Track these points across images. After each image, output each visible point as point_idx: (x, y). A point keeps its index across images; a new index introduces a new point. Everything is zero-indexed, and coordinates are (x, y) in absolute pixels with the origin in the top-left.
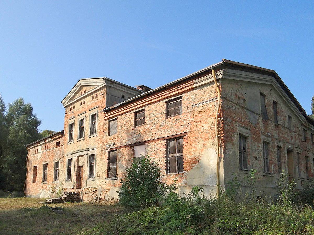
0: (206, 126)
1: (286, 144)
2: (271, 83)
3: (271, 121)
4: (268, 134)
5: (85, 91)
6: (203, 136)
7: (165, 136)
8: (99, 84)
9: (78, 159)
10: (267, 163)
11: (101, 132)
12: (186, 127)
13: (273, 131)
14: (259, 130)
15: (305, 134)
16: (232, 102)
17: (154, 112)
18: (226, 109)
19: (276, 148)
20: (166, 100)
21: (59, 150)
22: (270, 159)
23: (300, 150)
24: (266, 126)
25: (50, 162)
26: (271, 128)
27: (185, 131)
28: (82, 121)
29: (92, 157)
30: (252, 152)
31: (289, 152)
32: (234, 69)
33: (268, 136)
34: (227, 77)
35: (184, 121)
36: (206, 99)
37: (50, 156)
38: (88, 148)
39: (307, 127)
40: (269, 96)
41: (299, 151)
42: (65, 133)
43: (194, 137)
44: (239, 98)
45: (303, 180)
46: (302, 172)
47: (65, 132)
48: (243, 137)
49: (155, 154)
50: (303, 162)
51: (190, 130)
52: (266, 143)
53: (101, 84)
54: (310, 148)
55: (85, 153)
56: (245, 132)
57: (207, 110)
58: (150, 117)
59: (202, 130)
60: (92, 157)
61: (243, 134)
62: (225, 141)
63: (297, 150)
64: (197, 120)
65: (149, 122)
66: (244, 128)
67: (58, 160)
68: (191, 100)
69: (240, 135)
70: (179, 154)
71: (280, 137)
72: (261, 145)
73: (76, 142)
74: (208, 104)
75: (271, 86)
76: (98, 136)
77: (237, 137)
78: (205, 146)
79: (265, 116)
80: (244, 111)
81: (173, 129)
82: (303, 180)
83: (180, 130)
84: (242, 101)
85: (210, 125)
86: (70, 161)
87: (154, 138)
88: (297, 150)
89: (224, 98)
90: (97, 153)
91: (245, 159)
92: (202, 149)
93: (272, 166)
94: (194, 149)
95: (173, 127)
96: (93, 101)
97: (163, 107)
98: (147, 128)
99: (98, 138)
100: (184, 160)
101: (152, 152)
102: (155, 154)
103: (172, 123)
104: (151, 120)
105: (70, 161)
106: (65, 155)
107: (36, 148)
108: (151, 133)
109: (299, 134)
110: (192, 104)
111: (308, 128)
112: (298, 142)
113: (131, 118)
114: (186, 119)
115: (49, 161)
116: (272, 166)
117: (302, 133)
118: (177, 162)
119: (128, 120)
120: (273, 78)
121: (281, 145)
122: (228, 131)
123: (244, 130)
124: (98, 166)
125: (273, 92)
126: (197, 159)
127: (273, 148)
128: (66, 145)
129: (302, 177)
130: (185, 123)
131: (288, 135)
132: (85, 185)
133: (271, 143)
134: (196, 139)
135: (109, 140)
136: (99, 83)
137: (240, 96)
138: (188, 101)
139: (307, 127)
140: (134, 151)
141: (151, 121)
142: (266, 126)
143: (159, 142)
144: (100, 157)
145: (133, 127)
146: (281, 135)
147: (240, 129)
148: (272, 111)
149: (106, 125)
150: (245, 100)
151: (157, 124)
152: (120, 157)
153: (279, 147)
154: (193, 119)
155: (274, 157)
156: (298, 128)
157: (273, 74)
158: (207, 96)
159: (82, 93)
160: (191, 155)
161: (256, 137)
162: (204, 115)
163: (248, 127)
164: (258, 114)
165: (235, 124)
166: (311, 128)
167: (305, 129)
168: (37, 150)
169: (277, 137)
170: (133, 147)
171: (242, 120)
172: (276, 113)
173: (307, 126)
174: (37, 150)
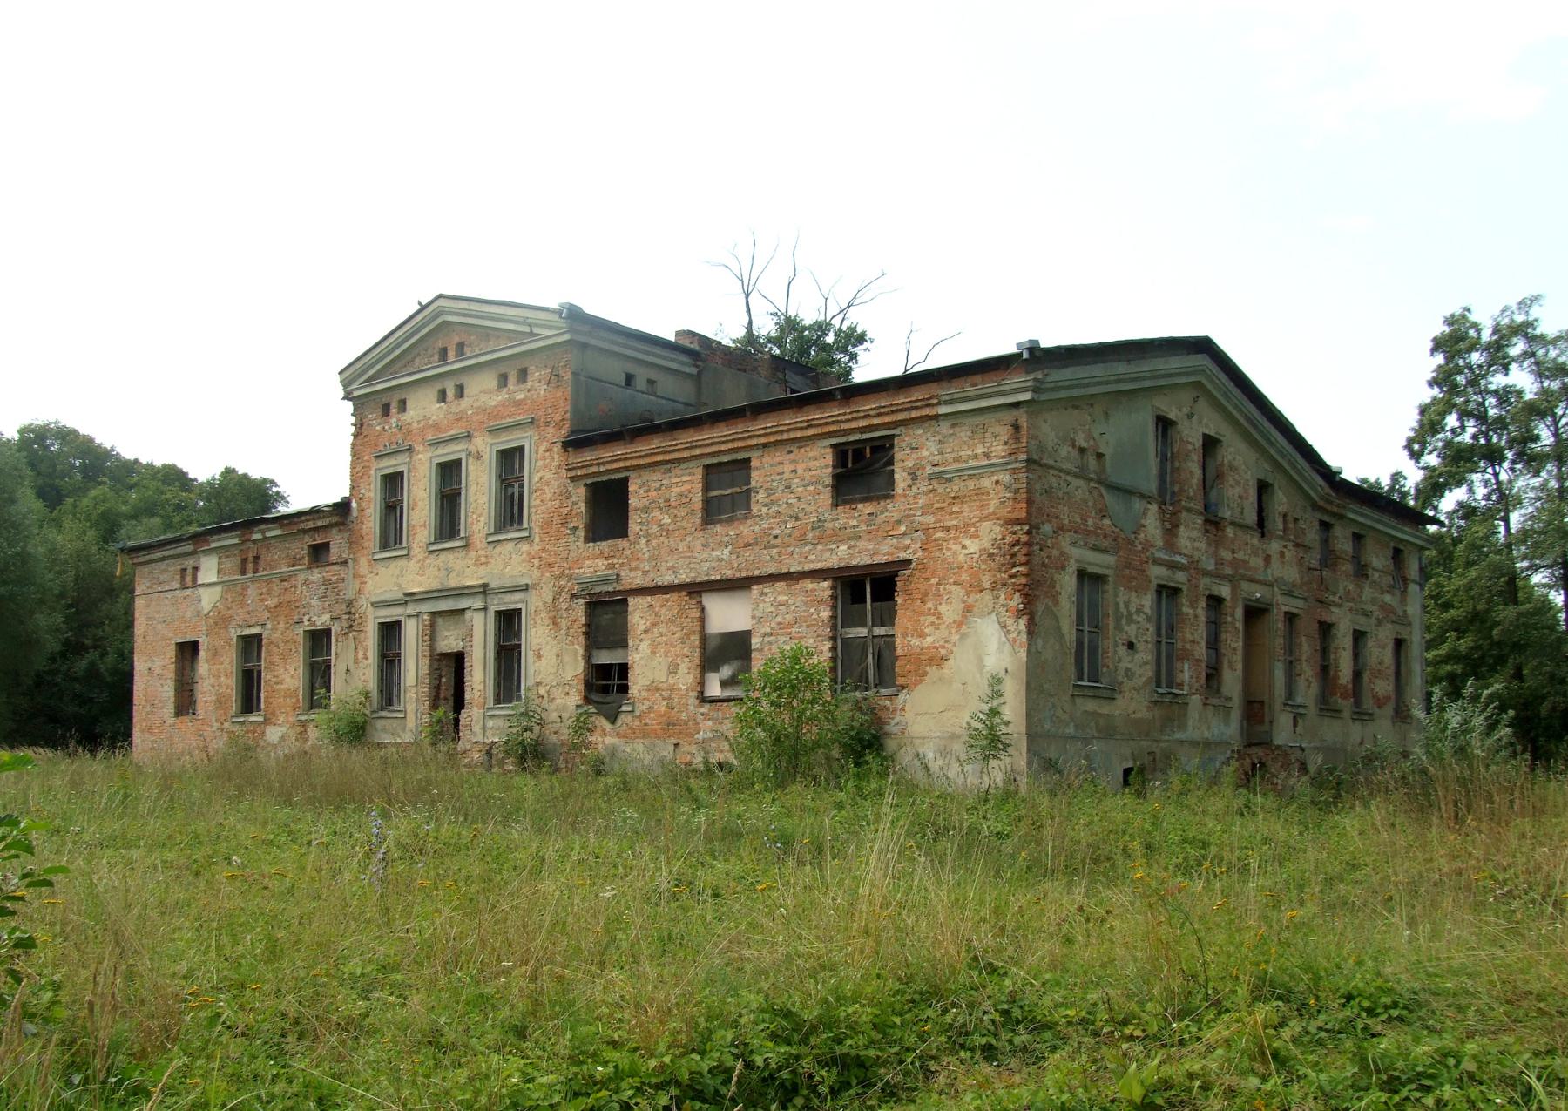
0: (973, 546)
1: (1245, 585)
2: (1192, 379)
3: (1189, 510)
4: (1178, 558)
5: (461, 347)
6: (965, 577)
7: (829, 565)
8: (536, 330)
9: (433, 625)
10: (1169, 657)
11: (549, 523)
12: (908, 541)
13: (1197, 544)
14: (1145, 550)
15: (1325, 542)
16: (1061, 470)
17: (786, 476)
18: (1037, 497)
19: (1203, 604)
20: (834, 441)
21: (326, 582)
22: (1179, 645)
23: (1300, 603)
24: (1171, 530)
25: (274, 629)
26: (1191, 537)
27: (903, 556)
28: (449, 471)
29: (509, 622)
30: (1118, 628)
31: (1255, 613)
32: (1066, 366)
33: (1172, 566)
34: (1044, 397)
35: (898, 522)
36: (975, 457)
37: (271, 603)
38: (485, 586)
39: (1334, 515)
40: (1186, 423)
41: (1296, 605)
42: (355, 514)
43: (934, 581)
44: (1082, 450)
45: (1301, 711)
46: (1301, 683)
47: (354, 505)
48: (1088, 579)
49: (790, 626)
50: (1307, 648)
51: (920, 554)
52: (1168, 593)
53: (548, 333)
54: (1341, 592)
55: (477, 602)
56: (1100, 562)
57: (980, 492)
58: (770, 491)
59: (961, 558)
60: (509, 622)
61: (1091, 569)
62: (1029, 600)
63: (1283, 604)
64: (948, 524)
65: (765, 510)
66: (1095, 548)
67: (322, 621)
68: (925, 453)
69: (1082, 575)
70: (879, 631)
71: (1220, 562)
72: (1148, 601)
73: (418, 551)
74: (981, 476)
75: (1198, 385)
76: (537, 539)
77: (1067, 583)
78: (968, 609)
79: (1167, 496)
80: (1095, 493)
81: (860, 544)
82: (1301, 711)
83: (885, 548)
84: (1092, 462)
85: (987, 545)
86: (390, 632)
87: (785, 570)
88: (1283, 604)
89: (1035, 462)
90: (534, 610)
91: (1094, 651)
92: (958, 618)
93: (1186, 666)
94: (933, 619)
95: (861, 539)
96: (503, 396)
97: (823, 462)
98: (757, 528)
99: (536, 548)
100: (899, 652)
101: (779, 619)
102: (790, 626)
103: (855, 523)
104: (773, 503)
105: (390, 632)
106: (363, 604)
107: (189, 563)
108: (775, 551)
109: (1297, 545)
110: (929, 470)
111: (1341, 517)
112: (1292, 574)
113: (687, 487)
114: (907, 517)
115: (269, 626)
116: (1186, 666)
117: (1312, 535)
118: (870, 657)
119: (675, 490)
120: (1202, 360)
121: (1225, 591)
122: (1043, 564)
123: (1091, 556)
124: (539, 657)
125: (1203, 406)
126: (943, 651)
127: (1193, 605)
128: (363, 562)
129: (1299, 700)
130: (903, 528)
131: (1255, 554)
132: (477, 728)
133: (1185, 588)
134: (939, 584)
135: (594, 563)
136: (537, 325)
137: (1085, 445)
138: (914, 456)
139: (1334, 515)
140: (703, 610)
141: (774, 509)
142: (1171, 530)
143: (809, 585)
144: (547, 621)
145: (698, 521)
146: (1226, 555)
147: (1079, 555)
148: (1198, 472)
149: (574, 499)
150: (1100, 456)
151: (797, 519)
152: (642, 627)
153: (1215, 602)
154: (930, 519)
155: (1195, 635)
156: (1296, 520)
157: (1204, 346)
158: (980, 450)
159: (444, 353)
160: (922, 636)
161: (1132, 574)
162: (968, 511)
163: (1105, 543)
164: (1142, 496)
165: (1065, 541)
166: (1352, 516)
167: (1326, 519)
168: (189, 571)
169: (1211, 567)
170: (699, 593)
171: (1090, 522)
172: (1212, 479)
173: (1335, 509)
174: (189, 571)
